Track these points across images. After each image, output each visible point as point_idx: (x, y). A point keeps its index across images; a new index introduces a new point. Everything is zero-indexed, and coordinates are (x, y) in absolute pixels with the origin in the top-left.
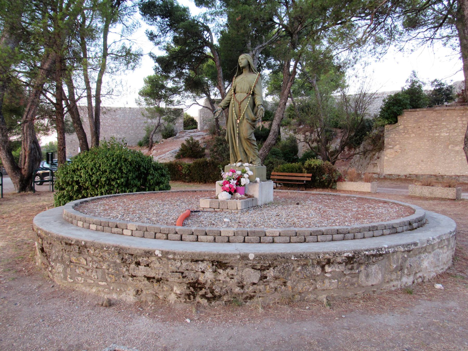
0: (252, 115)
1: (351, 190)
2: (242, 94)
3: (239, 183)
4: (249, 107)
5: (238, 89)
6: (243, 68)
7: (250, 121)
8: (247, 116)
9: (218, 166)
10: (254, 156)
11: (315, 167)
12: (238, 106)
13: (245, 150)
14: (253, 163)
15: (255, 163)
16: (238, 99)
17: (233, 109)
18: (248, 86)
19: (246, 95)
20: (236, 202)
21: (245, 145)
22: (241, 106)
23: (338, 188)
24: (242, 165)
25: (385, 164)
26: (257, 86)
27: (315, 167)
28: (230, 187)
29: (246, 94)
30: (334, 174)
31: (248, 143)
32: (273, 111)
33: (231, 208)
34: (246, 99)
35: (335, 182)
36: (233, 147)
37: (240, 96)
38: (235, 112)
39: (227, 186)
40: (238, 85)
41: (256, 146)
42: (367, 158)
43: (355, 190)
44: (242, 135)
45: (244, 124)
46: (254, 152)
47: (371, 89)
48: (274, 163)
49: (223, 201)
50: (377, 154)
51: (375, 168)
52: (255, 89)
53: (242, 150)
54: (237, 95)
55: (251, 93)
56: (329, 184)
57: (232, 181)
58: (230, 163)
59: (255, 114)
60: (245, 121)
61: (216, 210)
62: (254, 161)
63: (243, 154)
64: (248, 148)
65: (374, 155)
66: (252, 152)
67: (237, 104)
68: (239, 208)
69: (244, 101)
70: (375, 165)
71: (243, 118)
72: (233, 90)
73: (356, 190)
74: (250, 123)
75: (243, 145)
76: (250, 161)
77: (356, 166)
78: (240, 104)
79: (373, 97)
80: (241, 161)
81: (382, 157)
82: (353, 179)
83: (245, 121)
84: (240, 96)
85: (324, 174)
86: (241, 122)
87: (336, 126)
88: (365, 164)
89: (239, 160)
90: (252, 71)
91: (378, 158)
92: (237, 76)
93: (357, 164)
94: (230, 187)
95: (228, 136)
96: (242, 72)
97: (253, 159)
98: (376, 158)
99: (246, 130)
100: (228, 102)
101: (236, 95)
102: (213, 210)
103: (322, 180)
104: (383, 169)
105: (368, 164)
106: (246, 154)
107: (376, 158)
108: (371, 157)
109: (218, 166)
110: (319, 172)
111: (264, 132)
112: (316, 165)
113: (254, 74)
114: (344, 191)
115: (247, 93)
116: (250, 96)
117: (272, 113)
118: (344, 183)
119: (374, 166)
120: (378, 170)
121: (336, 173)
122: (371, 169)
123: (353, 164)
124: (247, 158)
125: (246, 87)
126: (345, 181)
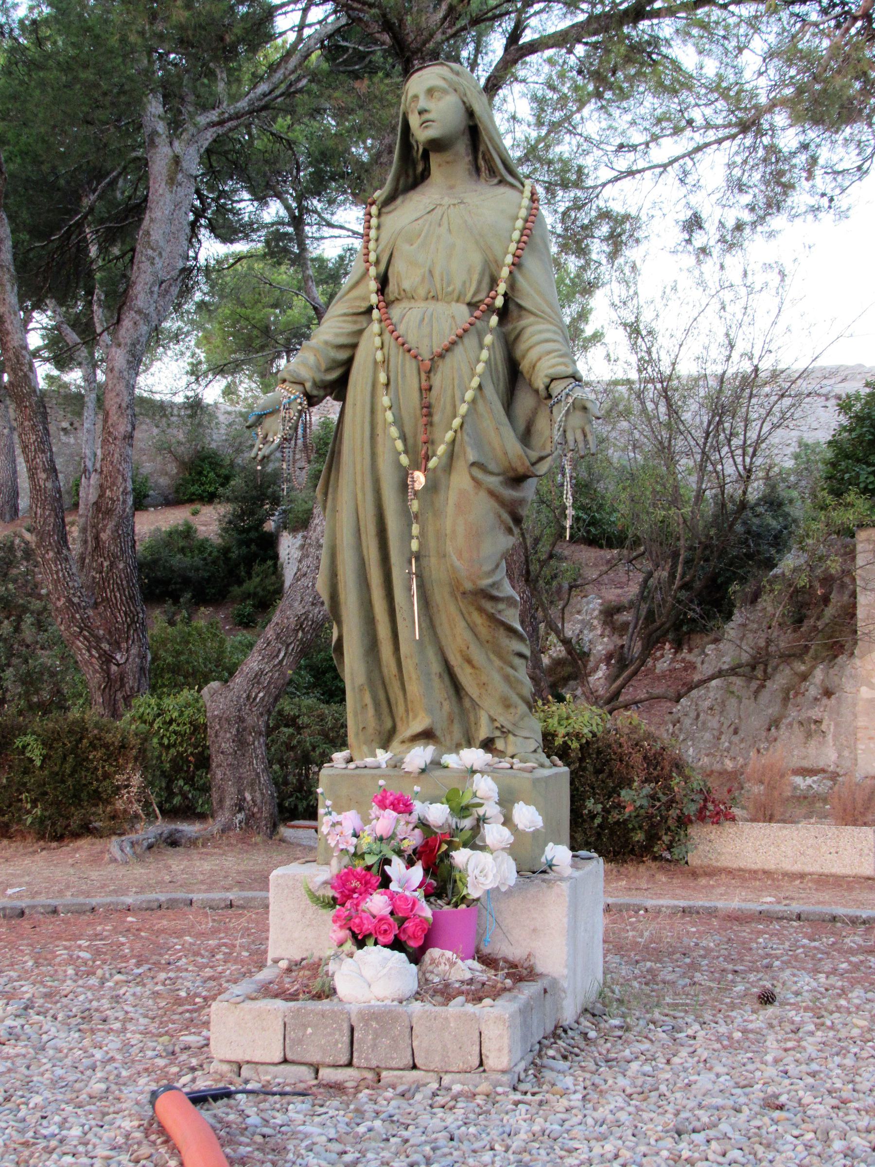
0: (506, 444)
1: (771, 866)
2: (439, 307)
3: (442, 882)
4: (490, 391)
5: (405, 276)
6: (437, 145)
7: (494, 481)
8: (479, 445)
9: (18, 743)
10: (507, 705)
11: (575, 745)
12: (411, 383)
13: (455, 661)
14: (500, 745)
15: (511, 745)
16: (412, 340)
17: (385, 401)
18: (476, 260)
19: (462, 312)
20: (474, 1018)
21: (457, 634)
22: (436, 380)
23: (694, 859)
24: (437, 763)
25: (862, 722)
26: (531, 263)
27: (575, 745)
28: (401, 913)
29: (464, 309)
30: (677, 783)
31: (478, 619)
32: (239, 451)
33: (436, 1064)
34: (470, 341)
35: (684, 822)
36: (372, 647)
37: (428, 321)
38: (398, 422)
39: (377, 903)
40: (404, 249)
41: (520, 638)
42: (765, 695)
43: (788, 866)
44: (436, 570)
45: (453, 496)
46: (507, 678)
47: (791, 355)
48: (303, 720)
49: (380, 1018)
50: (819, 674)
51: (813, 743)
52: (521, 282)
53: (436, 667)
54: (408, 317)
55: (499, 302)
56: (653, 837)
57: (396, 869)
58: (341, 743)
59: (526, 437)
60: (461, 479)
61: (326, 1074)
62: (505, 732)
63: (440, 690)
64: (477, 654)
65: (804, 677)
66: (497, 678)
67: (411, 367)
68: (497, 1060)
69: (459, 350)
70: (812, 729)
71: (451, 455)
72: (373, 285)
73: (797, 868)
74: (492, 494)
75: (444, 630)
76: (483, 733)
77: (707, 736)
78: (428, 369)
79: (790, 389)
80: (427, 736)
81: (848, 686)
82: (778, 810)
83: (461, 479)
84: (428, 321)
85: (628, 783)
86: (432, 487)
87: (595, 533)
88: (755, 723)
89: (418, 726)
90: (492, 171)
91: (828, 693)
92: (391, 199)
93: (713, 723)
94: (401, 913)
95: (333, 575)
96: (425, 175)
97: (502, 720)
98: (813, 691)
99: (466, 535)
100: (343, 355)
101: (396, 312)
102: (305, 1073)
103: (614, 816)
104: (854, 750)
105: (775, 723)
106: (457, 688)
107: (813, 691)
108: (786, 691)
109: (18, 743)
110: (598, 772)
111: (197, 561)
112: (578, 736)
113: (503, 190)
114: (729, 872)
115: (472, 305)
116: (494, 320)
117: (232, 465)
118: (729, 828)
119: (809, 735)
120: (827, 755)
121: (687, 779)
122: (790, 750)
123: (687, 722)
124: (460, 722)
125: (462, 269)
126: (733, 819)
